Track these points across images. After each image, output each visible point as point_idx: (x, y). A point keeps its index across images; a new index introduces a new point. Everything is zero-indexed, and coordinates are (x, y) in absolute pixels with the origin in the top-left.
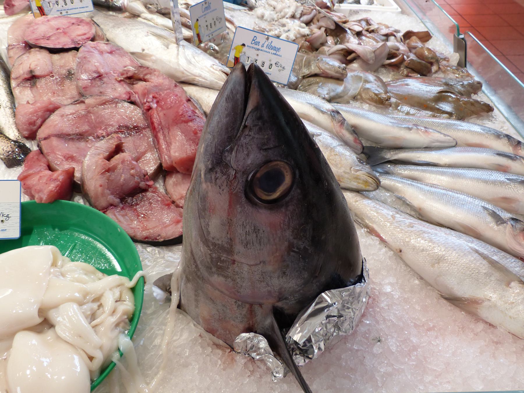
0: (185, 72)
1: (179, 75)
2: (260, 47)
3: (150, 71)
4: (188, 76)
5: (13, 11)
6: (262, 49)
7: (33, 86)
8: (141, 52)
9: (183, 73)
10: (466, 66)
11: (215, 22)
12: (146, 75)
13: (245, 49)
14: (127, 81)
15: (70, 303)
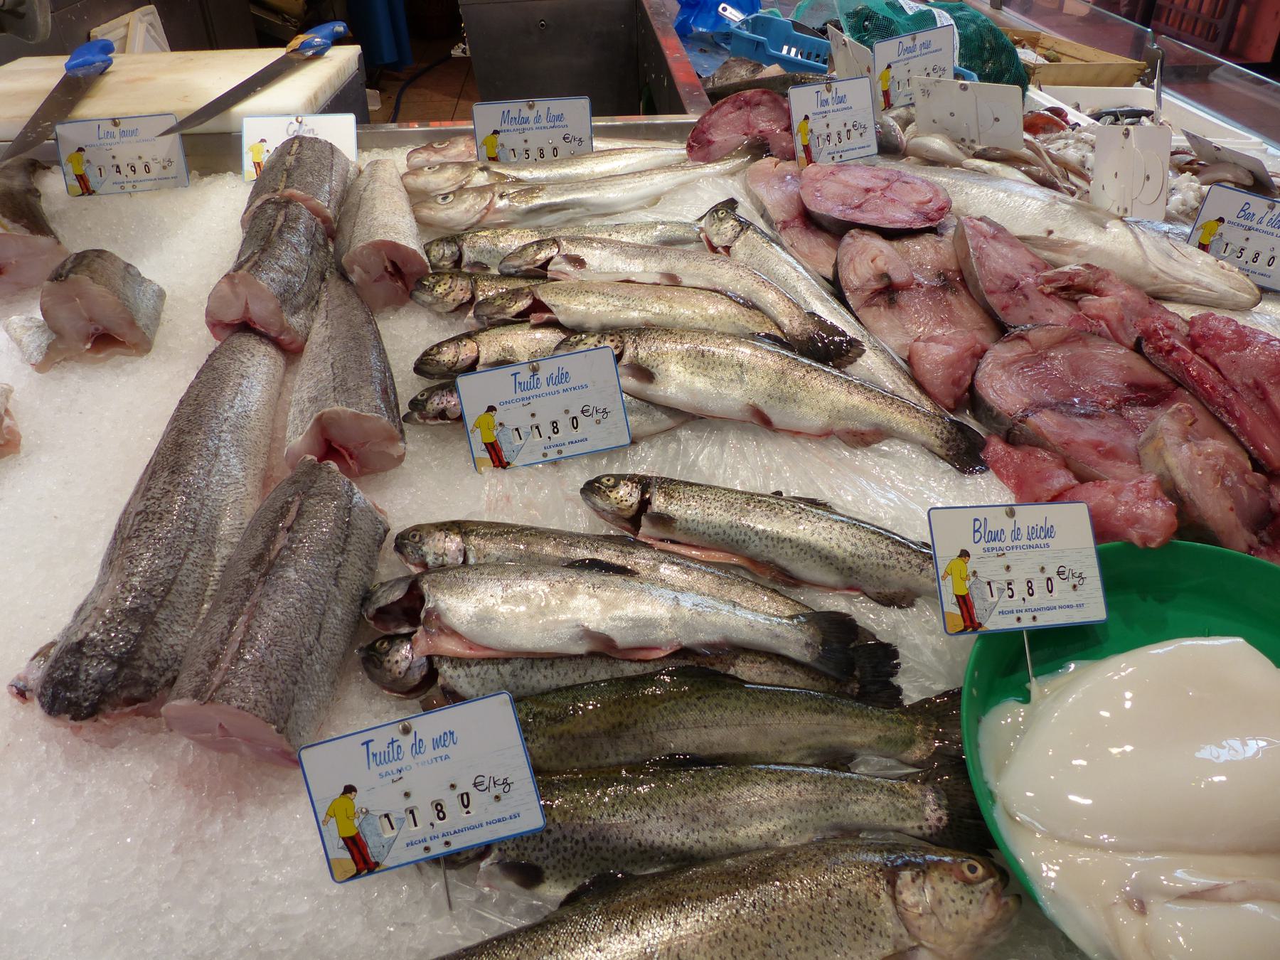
0: (1161, 275)
1: (1144, 280)
2: (1254, 224)
3: (1104, 275)
4: (1167, 282)
5: (709, 153)
6: (1259, 227)
7: (892, 303)
8: (1044, 235)
9: (1156, 277)
10: (403, 439)
11: (849, 131)
12: (1097, 281)
13: (1223, 228)
14: (1063, 294)
15: (1051, 909)
